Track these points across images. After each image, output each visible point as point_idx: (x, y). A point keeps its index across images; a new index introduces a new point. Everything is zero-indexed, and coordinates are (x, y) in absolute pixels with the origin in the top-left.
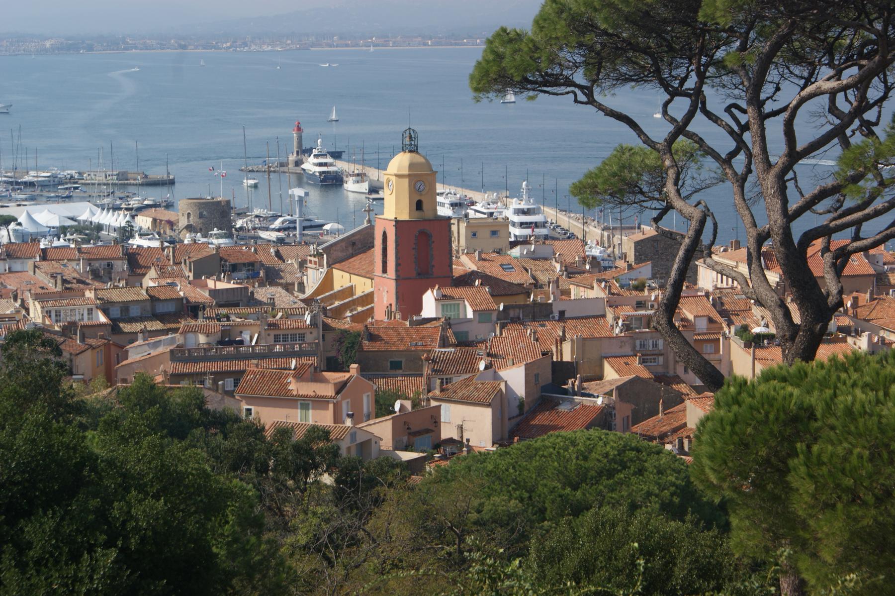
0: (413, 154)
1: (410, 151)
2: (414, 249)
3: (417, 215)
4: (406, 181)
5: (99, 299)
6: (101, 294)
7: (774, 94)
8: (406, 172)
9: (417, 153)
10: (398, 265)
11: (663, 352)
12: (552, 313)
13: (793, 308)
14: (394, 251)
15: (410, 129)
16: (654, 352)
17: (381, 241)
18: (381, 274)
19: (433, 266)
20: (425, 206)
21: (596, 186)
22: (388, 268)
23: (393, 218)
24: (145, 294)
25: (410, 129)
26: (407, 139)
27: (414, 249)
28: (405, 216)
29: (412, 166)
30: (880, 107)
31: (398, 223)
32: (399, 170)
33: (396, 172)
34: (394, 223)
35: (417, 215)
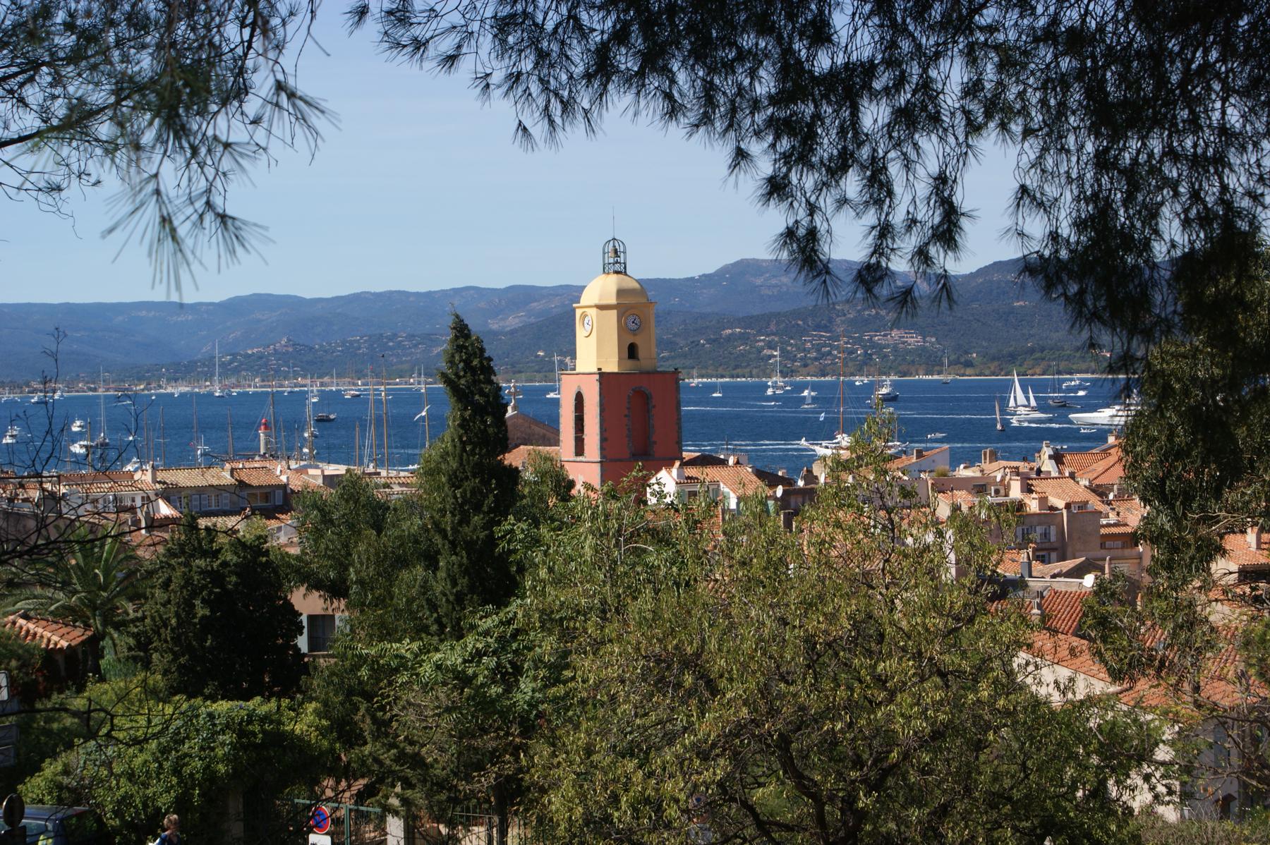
0: (620, 276)
1: (617, 272)
2: (626, 416)
3: (630, 365)
4: (613, 314)
5: (159, 482)
6: (161, 476)
7: (208, 198)
8: (613, 300)
9: (625, 274)
10: (603, 440)
11: (1056, 545)
13: (827, 12)
14: (597, 420)
15: (614, 239)
16: (1044, 546)
17: (573, 408)
18: (573, 458)
19: (655, 443)
20: (641, 353)
21: (835, 743)
22: (586, 447)
23: (595, 370)
24: (229, 477)
25: (614, 239)
26: (611, 254)
27: (626, 416)
28: (612, 367)
29: (621, 293)
30: (33, 168)
31: (604, 377)
32: (601, 297)
33: (597, 302)
34: (597, 377)
35: (630, 365)
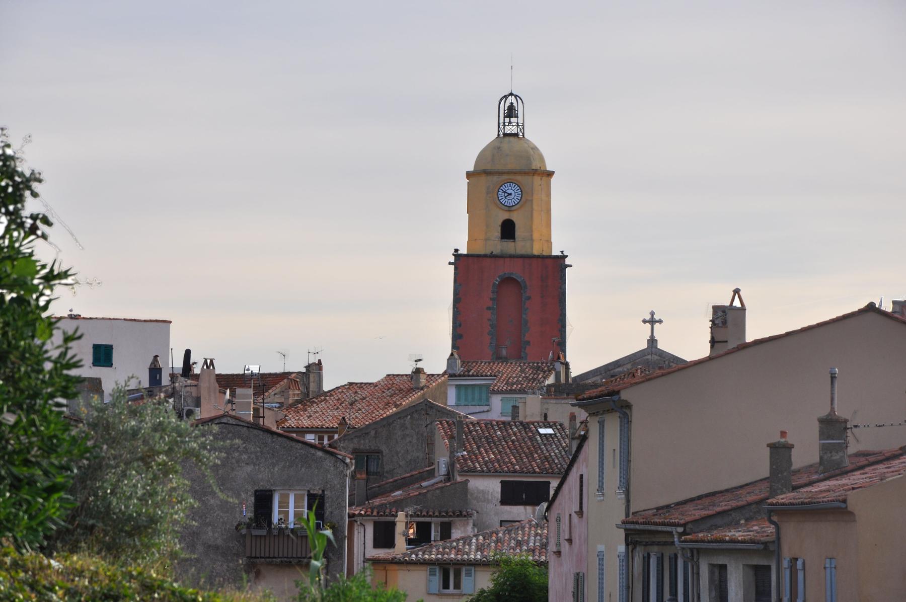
2: (489, 308)
3: (497, 246)
15: (511, 94)
27: (489, 308)
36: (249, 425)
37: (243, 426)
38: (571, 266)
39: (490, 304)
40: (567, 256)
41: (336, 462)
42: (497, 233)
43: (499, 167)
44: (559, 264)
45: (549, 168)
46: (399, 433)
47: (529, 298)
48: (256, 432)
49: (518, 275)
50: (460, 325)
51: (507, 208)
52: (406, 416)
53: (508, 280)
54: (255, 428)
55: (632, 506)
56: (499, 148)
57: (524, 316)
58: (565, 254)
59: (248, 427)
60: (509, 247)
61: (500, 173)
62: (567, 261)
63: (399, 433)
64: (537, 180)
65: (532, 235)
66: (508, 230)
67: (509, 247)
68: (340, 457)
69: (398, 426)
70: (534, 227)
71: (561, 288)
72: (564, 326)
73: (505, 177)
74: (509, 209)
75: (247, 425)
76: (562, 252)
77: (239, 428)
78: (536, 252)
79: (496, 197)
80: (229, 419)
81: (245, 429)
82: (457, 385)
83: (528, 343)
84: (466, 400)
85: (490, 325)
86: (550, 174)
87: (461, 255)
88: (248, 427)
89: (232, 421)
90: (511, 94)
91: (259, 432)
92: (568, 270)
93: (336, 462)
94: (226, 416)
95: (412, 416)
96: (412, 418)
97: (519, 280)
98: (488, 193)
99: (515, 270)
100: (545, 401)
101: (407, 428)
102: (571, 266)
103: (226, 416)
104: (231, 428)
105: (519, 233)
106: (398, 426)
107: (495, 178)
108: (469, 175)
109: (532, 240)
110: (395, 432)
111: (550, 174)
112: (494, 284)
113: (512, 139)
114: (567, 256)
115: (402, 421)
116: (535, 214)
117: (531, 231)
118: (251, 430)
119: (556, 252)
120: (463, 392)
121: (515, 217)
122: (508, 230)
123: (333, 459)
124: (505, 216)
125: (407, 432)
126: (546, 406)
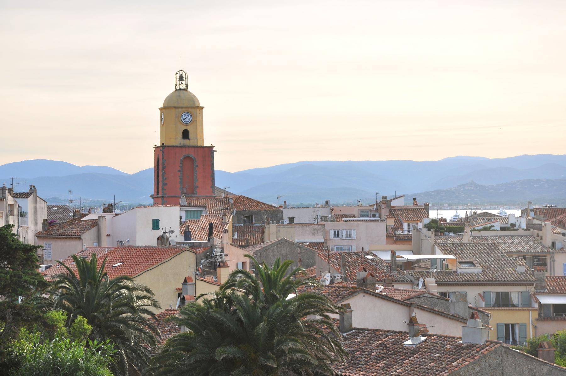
2: (179, 171)
3: (179, 140)
12: (282, 219)
27: (179, 171)
35: (179, 140)
36: (438, 298)
37: (435, 298)
38: (216, 151)
39: (180, 169)
40: (214, 147)
41: (484, 316)
42: (181, 135)
43: (180, 105)
44: (210, 150)
45: (201, 105)
46: (272, 254)
47: (197, 166)
48: (442, 301)
49: (192, 156)
50: (166, 179)
51: (185, 124)
52: (275, 246)
53: (187, 158)
54: (442, 299)
55: (96, 234)
56: (179, 96)
57: (195, 174)
58: (213, 146)
59: (438, 299)
60: (186, 142)
61: (182, 108)
62: (214, 149)
63: (272, 254)
64: (198, 110)
65: (197, 137)
66: (186, 134)
67: (186, 142)
68: (486, 314)
69: (271, 251)
70: (198, 133)
71: (212, 161)
72: (214, 179)
73: (184, 110)
74: (187, 124)
75: (437, 297)
76: (212, 145)
77: (433, 299)
78: (199, 145)
79: (180, 119)
80: (428, 294)
81: (436, 299)
82: (186, 211)
83: (197, 187)
84: (191, 217)
85: (180, 179)
86: (203, 108)
87: (158, 147)
88: (438, 299)
89: (429, 296)
90: (181, 70)
91: (444, 301)
92: (215, 153)
93: (484, 316)
94: (427, 293)
95: (277, 246)
96: (277, 247)
97: (193, 158)
98: (176, 117)
99: (186, 152)
100: (278, 226)
101: (275, 252)
102: (216, 151)
103: (427, 293)
104: (429, 299)
105: (191, 135)
106: (271, 251)
107: (179, 110)
108: (160, 109)
109: (197, 139)
110: (270, 253)
111: (203, 108)
112: (181, 160)
113: (184, 91)
114: (214, 147)
115: (273, 248)
116: (198, 126)
117: (197, 135)
118: (439, 300)
119: (207, 144)
120: (189, 213)
121: (189, 128)
122: (186, 134)
123: (482, 315)
124: (184, 128)
125: (275, 254)
126: (279, 229)
